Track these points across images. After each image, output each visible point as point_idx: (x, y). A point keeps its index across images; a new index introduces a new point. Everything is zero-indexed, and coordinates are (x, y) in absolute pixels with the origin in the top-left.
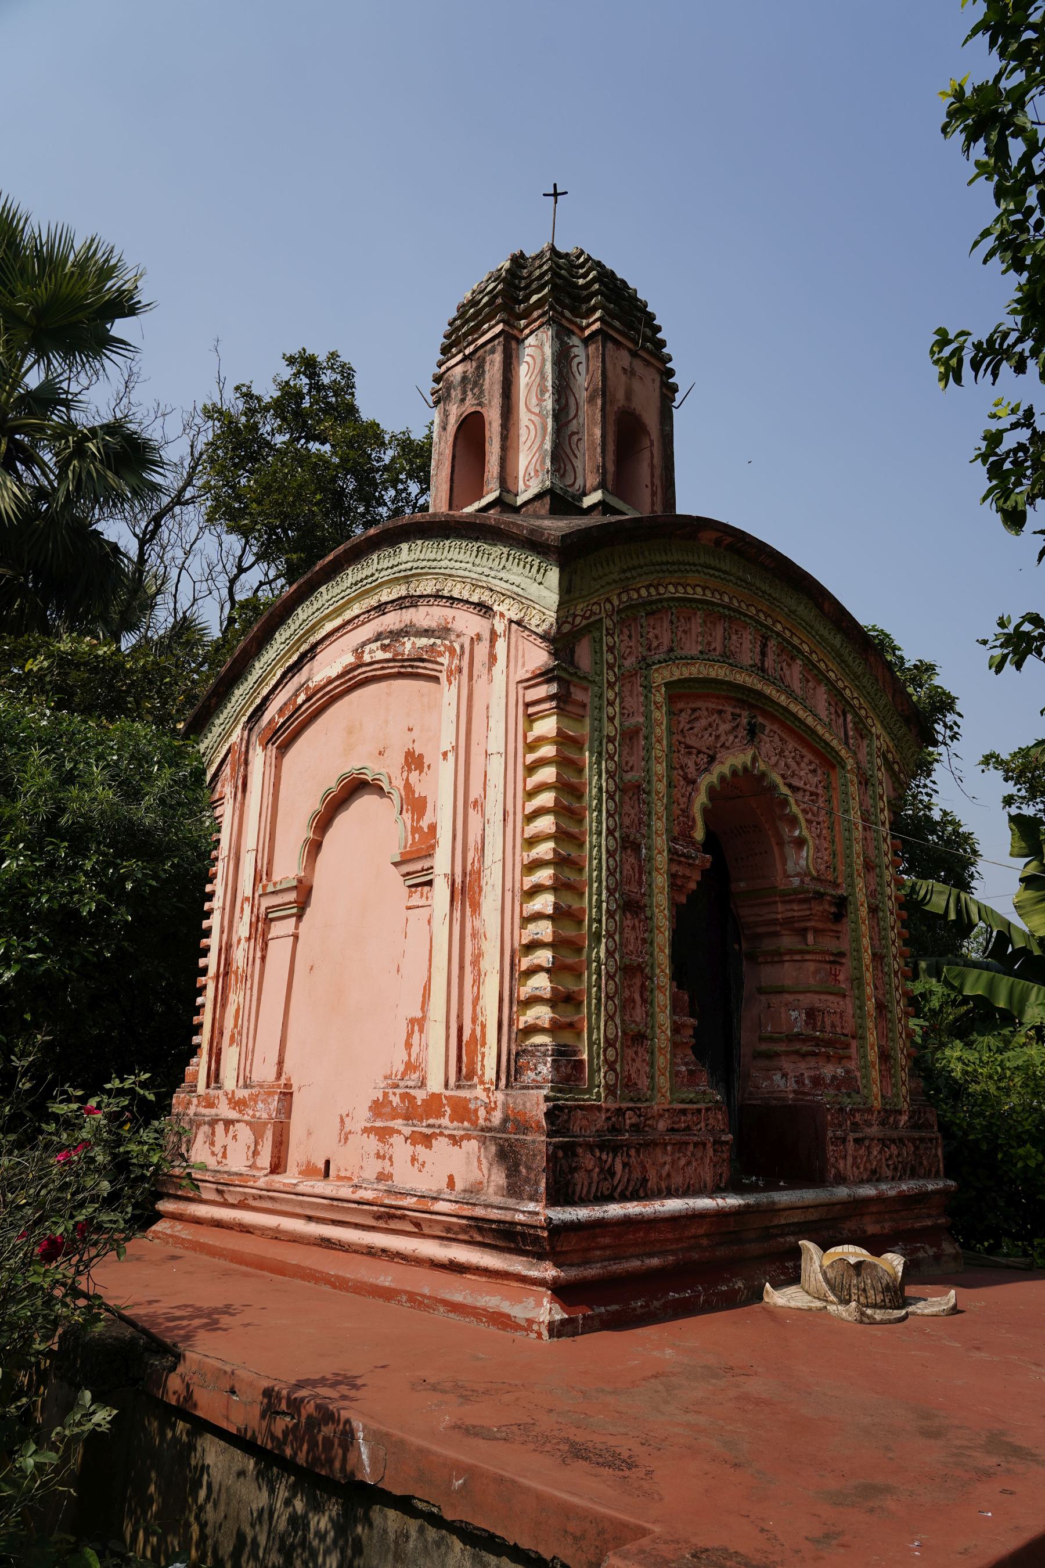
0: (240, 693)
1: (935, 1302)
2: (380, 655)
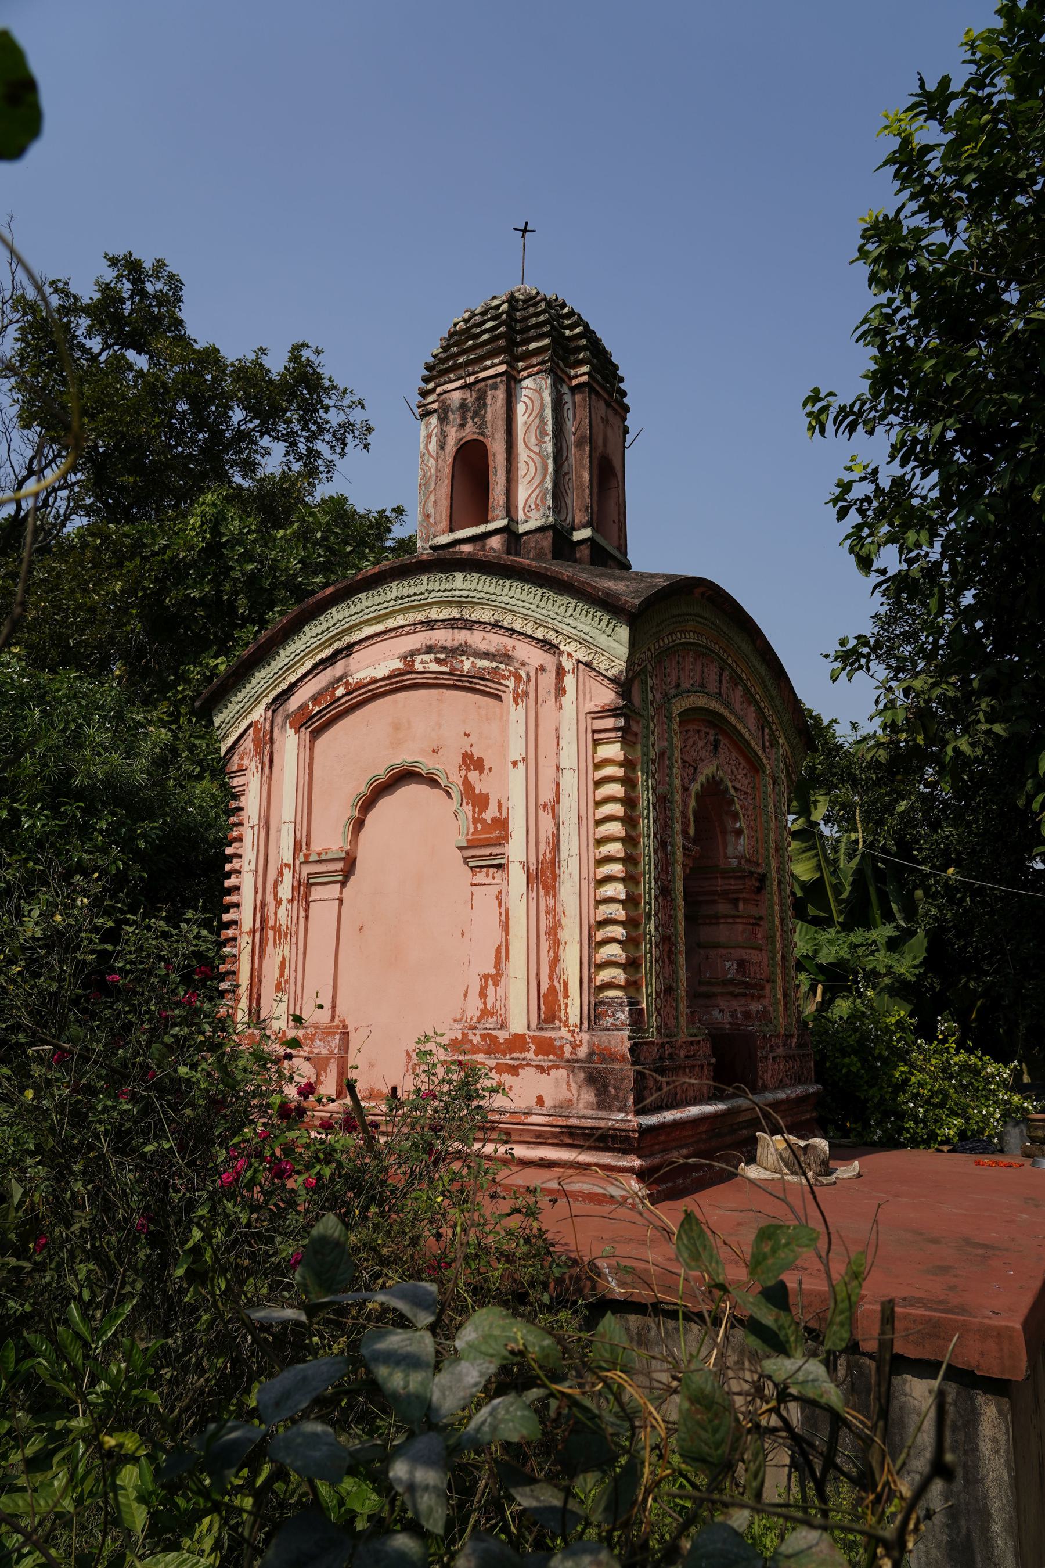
0: (261, 677)
1: (848, 1170)
2: (434, 667)
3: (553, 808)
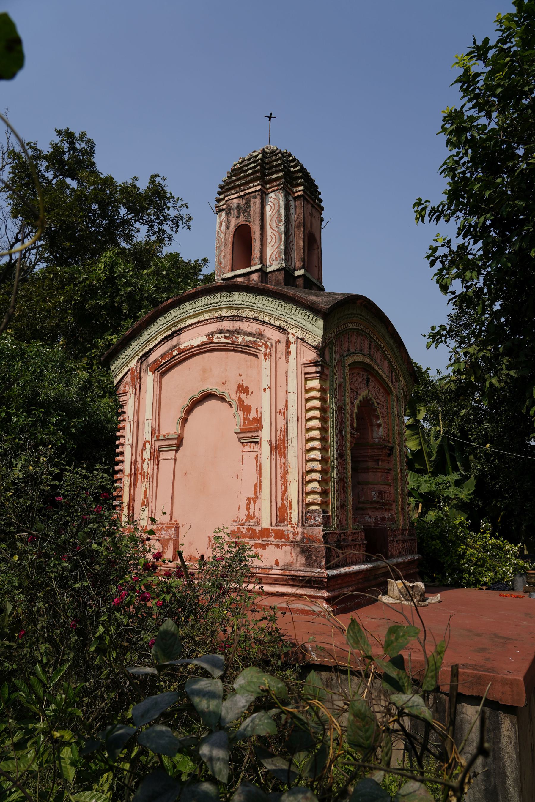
0: (135, 345)
1: (434, 599)
2: (223, 340)
3: (284, 413)
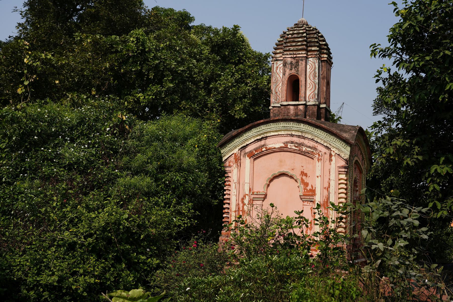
0: (237, 141)
2: (294, 148)
3: (327, 189)
